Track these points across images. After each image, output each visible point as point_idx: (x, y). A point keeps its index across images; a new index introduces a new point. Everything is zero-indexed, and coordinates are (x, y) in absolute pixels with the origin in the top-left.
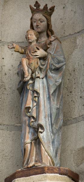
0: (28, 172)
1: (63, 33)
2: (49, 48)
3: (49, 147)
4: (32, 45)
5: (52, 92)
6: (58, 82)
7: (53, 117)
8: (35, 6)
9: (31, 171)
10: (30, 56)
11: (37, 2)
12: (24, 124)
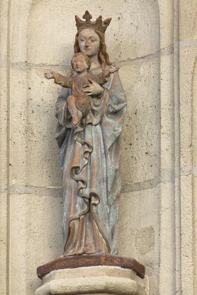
0: (76, 261)
1: (118, 57)
2: (106, 82)
3: (105, 225)
4: (81, 76)
5: (109, 146)
6: (117, 132)
7: (110, 182)
8: (85, 18)
9: (79, 261)
10: (80, 92)
11: (87, 13)
12: (69, 191)
